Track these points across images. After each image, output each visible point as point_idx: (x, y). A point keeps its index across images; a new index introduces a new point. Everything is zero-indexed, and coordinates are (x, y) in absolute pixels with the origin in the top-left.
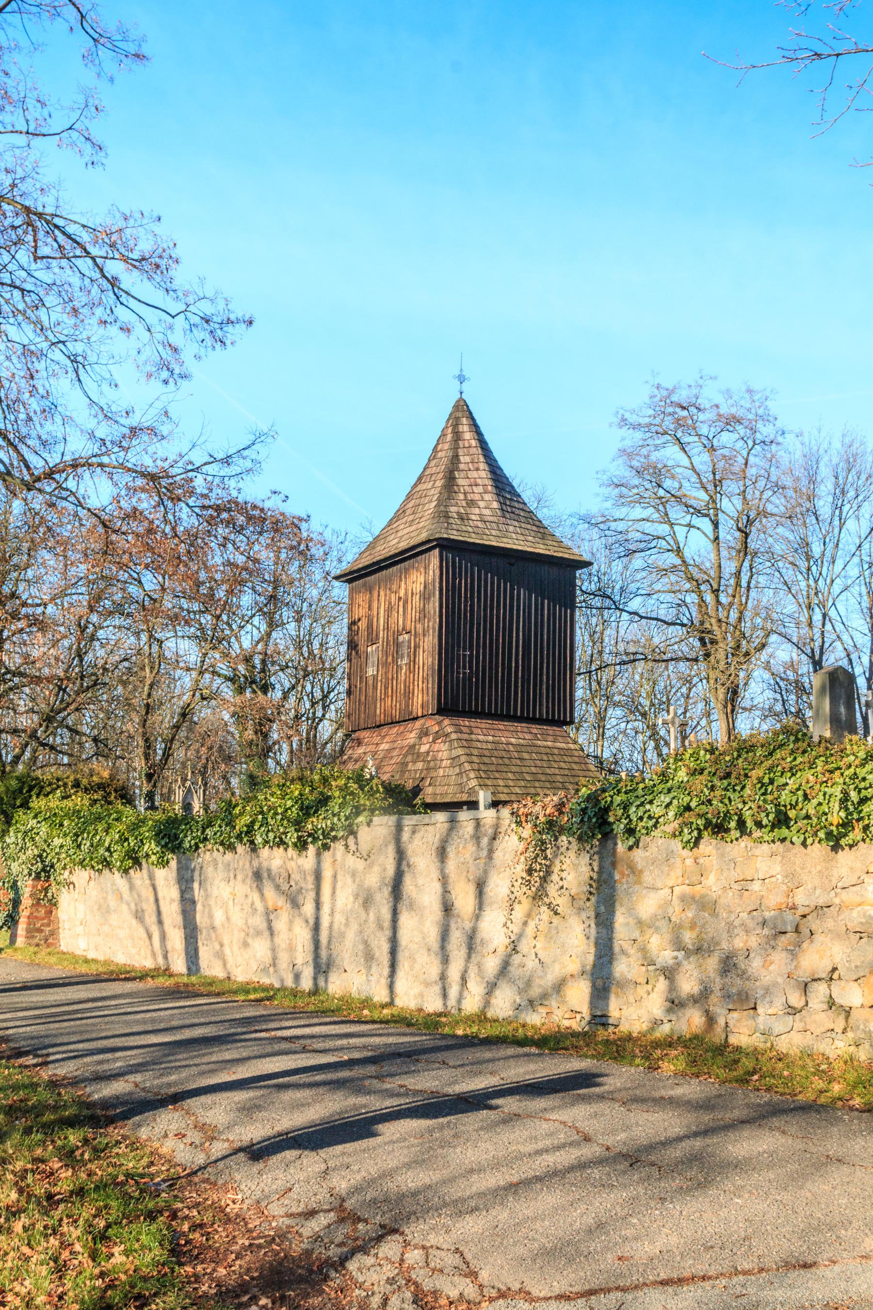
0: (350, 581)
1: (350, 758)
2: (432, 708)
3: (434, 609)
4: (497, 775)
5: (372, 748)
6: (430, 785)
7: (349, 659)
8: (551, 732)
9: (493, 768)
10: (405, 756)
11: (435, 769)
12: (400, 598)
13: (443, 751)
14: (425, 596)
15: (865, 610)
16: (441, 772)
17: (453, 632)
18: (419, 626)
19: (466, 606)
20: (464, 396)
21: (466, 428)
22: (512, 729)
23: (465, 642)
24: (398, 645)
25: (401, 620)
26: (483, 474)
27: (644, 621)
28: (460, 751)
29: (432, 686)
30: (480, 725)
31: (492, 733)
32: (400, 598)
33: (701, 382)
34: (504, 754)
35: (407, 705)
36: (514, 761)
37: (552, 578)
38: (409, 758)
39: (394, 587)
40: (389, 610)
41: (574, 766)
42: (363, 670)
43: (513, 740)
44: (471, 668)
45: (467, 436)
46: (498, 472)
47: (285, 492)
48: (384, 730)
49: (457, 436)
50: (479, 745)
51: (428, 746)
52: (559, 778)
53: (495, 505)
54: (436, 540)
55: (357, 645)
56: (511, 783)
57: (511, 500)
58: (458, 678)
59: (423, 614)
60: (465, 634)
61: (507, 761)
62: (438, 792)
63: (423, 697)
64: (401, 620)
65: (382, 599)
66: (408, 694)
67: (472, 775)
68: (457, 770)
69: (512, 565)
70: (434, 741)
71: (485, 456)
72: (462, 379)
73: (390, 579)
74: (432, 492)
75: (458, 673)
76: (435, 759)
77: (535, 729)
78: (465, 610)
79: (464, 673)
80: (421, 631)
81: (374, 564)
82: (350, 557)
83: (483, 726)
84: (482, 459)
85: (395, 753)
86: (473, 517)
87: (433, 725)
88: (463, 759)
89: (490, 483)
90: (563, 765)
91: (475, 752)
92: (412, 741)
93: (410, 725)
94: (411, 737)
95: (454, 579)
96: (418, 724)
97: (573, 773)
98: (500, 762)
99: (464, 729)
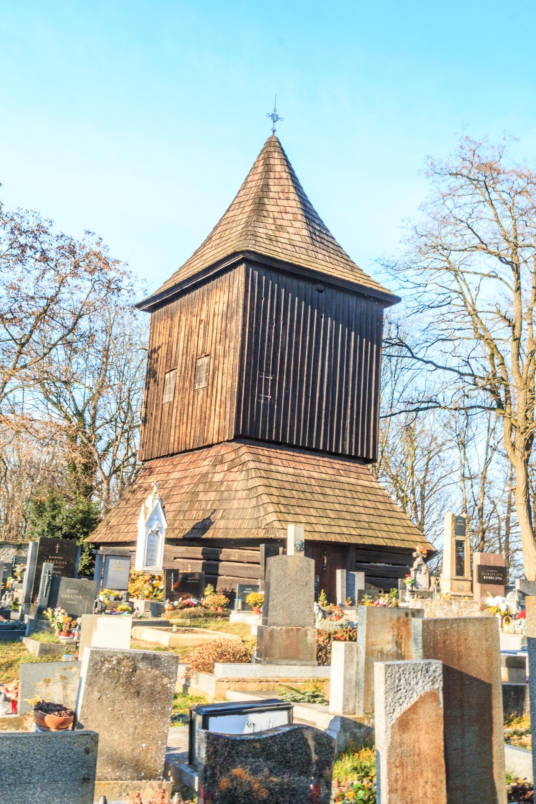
0: (152, 309)
1: (140, 487)
2: (229, 434)
3: (237, 327)
4: (298, 510)
5: (163, 477)
6: (222, 518)
7: (147, 388)
8: (353, 469)
9: (294, 502)
10: (196, 485)
11: (228, 500)
12: (201, 321)
13: (239, 480)
14: (227, 317)
15: (297, 546)
16: (235, 504)
17: (256, 353)
18: (220, 348)
19: (270, 328)
20: (276, 134)
21: (277, 162)
22: (313, 462)
23: (268, 365)
24: (196, 369)
25: (201, 343)
26: (293, 204)
27: (440, 371)
28: (258, 482)
29: (231, 411)
30: (280, 456)
31: (293, 464)
32: (201, 321)
33: (504, 143)
34: (305, 488)
35: (202, 431)
36: (316, 496)
37: (359, 308)
38: (201, 487)
39: (195, 311)
40: (190, 333)
41: (379, 506)
42: (159, 397)
43: (315, 475)
44: (273, 394)
45: (279, 168)
46: (308, 205)
47: (99, 234)
48: (177, 458)
49: (268, 168)
50: (279, 476)
51: (222, 474)
52: (364, 518)
53: (305, 232)
54: (242, 252)
55: (156, 373)
56: (313, 520)
57: (320, 231)
58: (259, 403)
59: (225, 334)
60: (268, 358)
61: (309, 496)
62: (231, 526)
63: (221, 420)
64: (201, 343)
65: (183, 323)
66: (204, 420)
67: (271, 508)
68: (254, 502)
69: (321, 292)
70: (229, 470)
71: (296, 188)
72: (275, 118)
73: (192, 303)
74: (241, 217)
75: (259, 398)
76: (229, 490)
77: (338, 464)
78: (270, 332)
79: (266, 399)
80: (221, 353)
81: (176, 286)
82: (155, 283)
83: (283, 457)
84: (292, 190)
85: (186, 482)
86: (282, 240)
87: (228, 451)
88: (261, 490)
89: (301, 212)
90: (367, 503)
91: (274, 483)
92: (205, 470)
93: (205, 452)
94: (205, 466)
95: (260, 299)
96: (213, 451)
97: (379, 512)
98: (302, 496)
99: (264, 459)
